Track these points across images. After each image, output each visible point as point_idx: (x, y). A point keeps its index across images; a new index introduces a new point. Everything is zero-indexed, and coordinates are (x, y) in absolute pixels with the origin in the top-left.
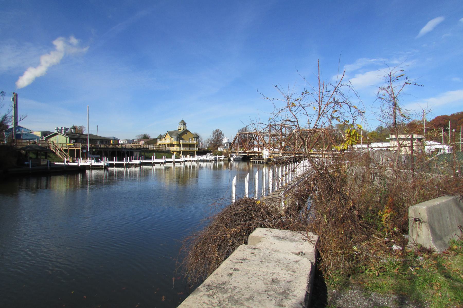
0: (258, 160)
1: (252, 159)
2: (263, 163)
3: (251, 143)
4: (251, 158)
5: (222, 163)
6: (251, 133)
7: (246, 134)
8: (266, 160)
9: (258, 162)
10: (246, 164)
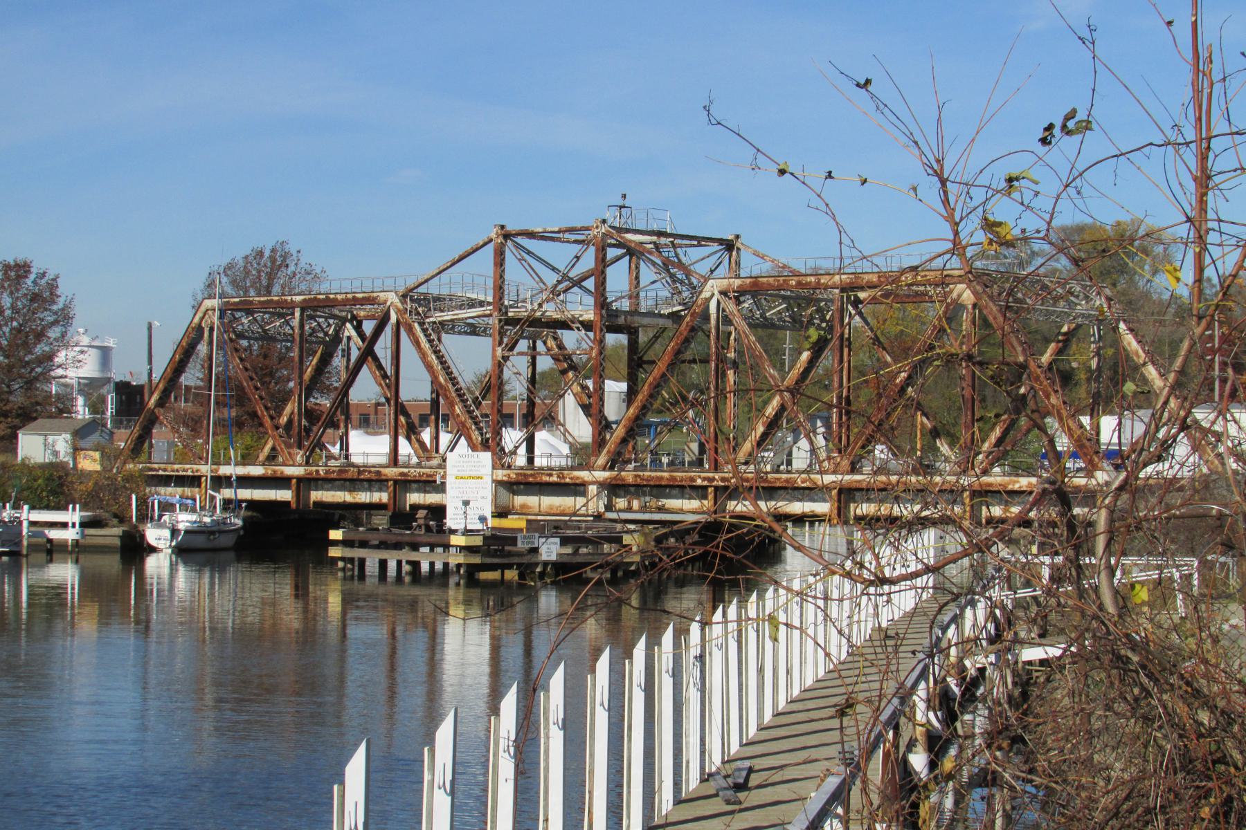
0: (398, 546)
1: (346, 543)
2: (440, 578)
3: (326, 390)
5: (65, 573)
6: (329, 303)
7: (282, 310)
9: (392, 565)
10: (281, 586)
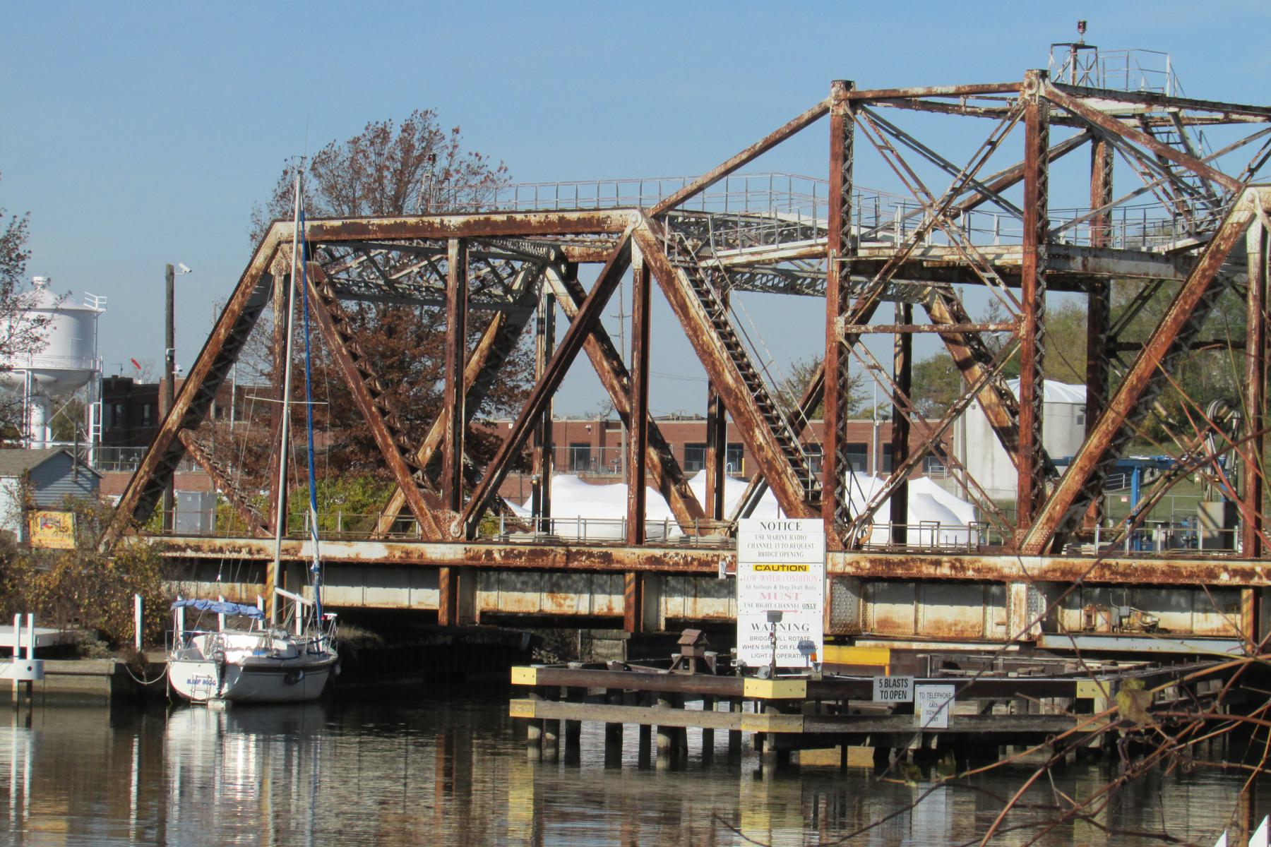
0: (643, 698)
1: (544, 692)
4: (523, 675)
6: (514, 231)
8: (781, 706)
9: (631, 737)
